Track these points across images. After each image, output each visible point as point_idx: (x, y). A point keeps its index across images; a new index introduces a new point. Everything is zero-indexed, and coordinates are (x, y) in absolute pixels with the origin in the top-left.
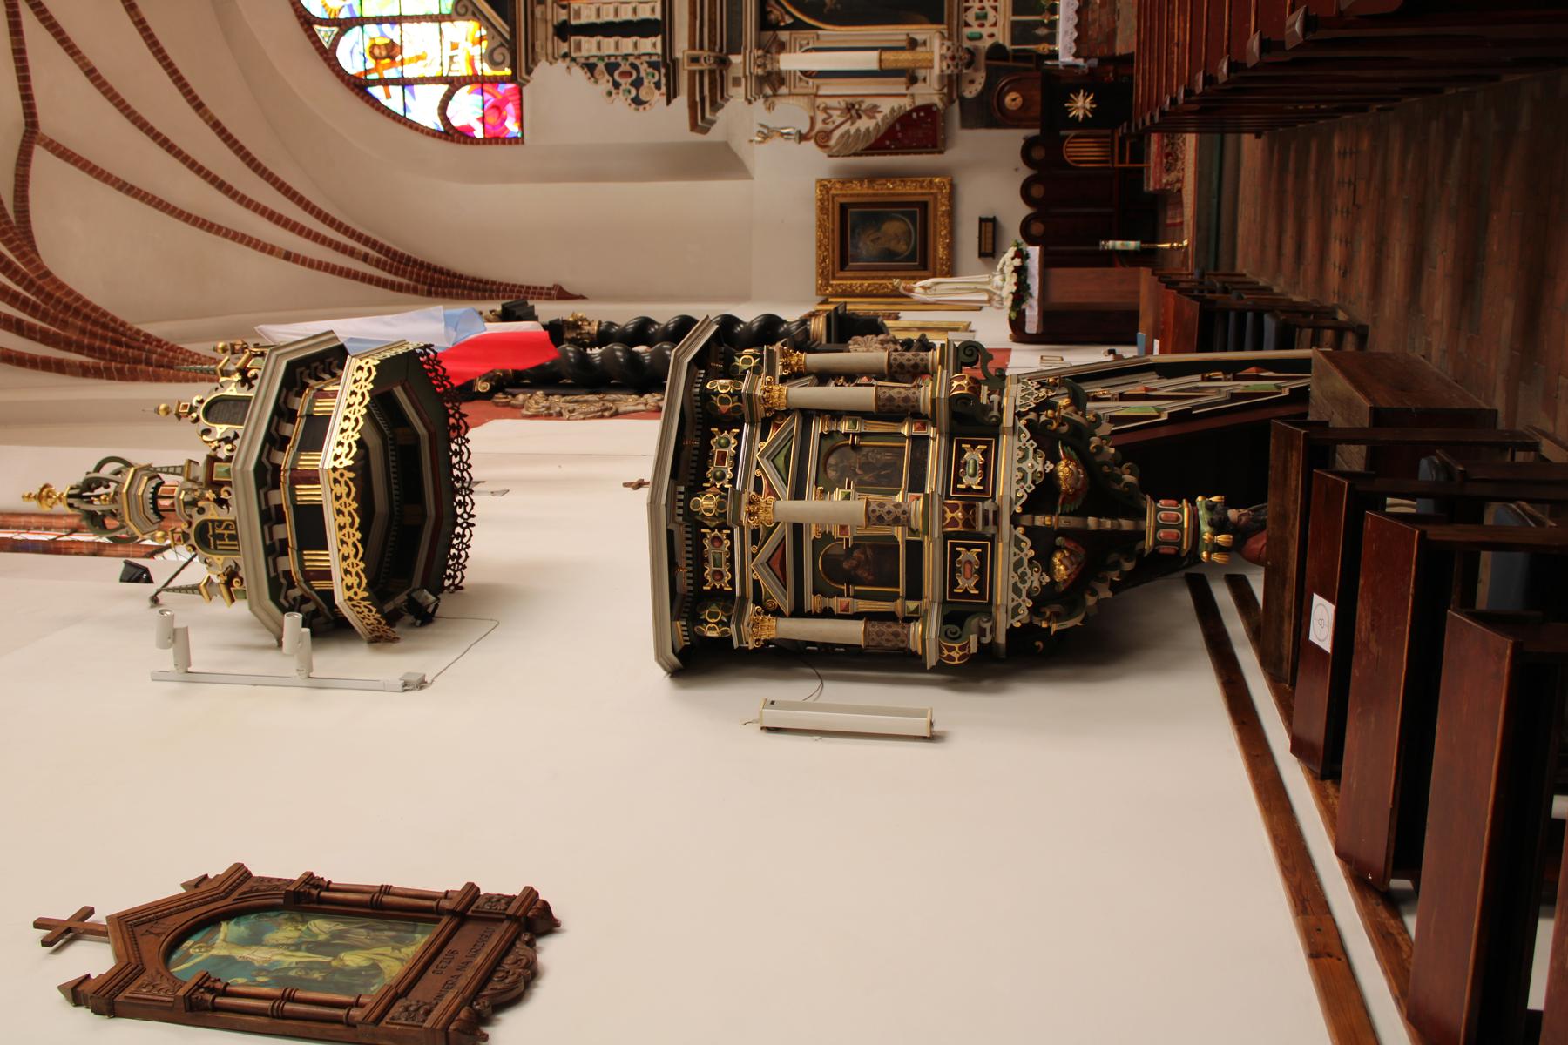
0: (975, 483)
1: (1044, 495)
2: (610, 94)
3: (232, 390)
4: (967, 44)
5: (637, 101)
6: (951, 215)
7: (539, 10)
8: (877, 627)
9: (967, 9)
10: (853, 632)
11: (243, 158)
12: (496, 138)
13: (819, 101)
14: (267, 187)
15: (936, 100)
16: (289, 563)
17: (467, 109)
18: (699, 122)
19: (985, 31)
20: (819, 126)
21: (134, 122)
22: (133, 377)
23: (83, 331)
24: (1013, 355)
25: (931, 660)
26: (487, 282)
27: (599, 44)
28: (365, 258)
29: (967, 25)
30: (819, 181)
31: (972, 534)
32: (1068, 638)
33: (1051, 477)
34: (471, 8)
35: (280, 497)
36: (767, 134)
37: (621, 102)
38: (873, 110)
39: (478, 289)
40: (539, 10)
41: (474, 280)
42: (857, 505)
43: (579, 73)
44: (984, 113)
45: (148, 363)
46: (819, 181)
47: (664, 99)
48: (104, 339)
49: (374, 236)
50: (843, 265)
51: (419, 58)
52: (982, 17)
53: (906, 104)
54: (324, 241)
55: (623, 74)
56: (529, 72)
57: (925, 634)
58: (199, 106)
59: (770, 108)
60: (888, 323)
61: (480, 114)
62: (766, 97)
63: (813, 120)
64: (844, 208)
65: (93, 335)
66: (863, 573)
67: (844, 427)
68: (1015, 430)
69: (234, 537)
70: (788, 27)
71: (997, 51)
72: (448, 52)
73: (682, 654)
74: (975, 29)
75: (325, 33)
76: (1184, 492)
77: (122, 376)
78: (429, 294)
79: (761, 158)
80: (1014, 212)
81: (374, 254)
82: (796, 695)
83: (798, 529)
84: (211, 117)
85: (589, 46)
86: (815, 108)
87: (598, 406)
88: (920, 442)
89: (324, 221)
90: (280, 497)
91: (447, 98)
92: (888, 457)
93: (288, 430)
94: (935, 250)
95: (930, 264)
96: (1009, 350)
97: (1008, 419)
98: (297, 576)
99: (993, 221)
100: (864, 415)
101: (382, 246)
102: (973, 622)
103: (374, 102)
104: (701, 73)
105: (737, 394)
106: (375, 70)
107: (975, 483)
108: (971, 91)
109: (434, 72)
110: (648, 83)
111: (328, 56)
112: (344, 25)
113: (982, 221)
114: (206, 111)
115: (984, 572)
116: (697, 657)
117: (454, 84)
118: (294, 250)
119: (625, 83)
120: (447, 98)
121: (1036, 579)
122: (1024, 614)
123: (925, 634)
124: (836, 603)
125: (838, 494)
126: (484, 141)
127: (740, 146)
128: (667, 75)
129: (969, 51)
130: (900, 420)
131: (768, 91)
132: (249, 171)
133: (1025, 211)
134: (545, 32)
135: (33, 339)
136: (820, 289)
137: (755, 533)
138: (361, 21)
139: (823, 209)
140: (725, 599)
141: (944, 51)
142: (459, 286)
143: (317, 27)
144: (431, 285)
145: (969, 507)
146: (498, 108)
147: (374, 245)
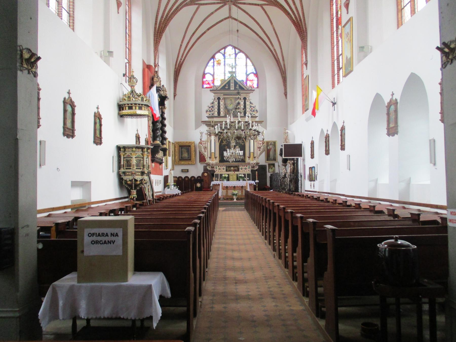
1: (136, 180)
3: (144, 99)
4: (215, 167)
5: (207, 111)
6: (189, 164)
7: (222, 95)
10: (122, 163)
17: (208, 78)
18: (204, 122)
19: (217, 170)
22: (154, 36)
28: (181, 59)
31: (132, 174)
32: (122, 183)
35: (133, 105)
36: (201, 133)
37: (207, 108)
38: (205, 151)
40: (222, 95)
43: (212, 101)
44: (206, 170)
50: (180, 146)
52: (220, 169)
53: (206, 157)
57: (122, 170)
58: (208, 29)
64: (190, 146)
71: (214, 171)
75: (222, 51)
76: (137, 194)
77: (155, 34)
80: (190, 175)
81: (182, 61)
85: (216, 103)
86: (206, 142)
88: (141, 169)
90: (133, 105)
91: (211, 74)
96: (162, 175)
99: (188, 171)
103: (210, 60)
108: (208, 168)
110: (210, 113)
111: (219, 51)
112: (224, 55)
116: (119, 148)
117: (213, 76)
120: (211, 74)
121: (128, 180)
123: (122, 170)
139: (190, 143)
140: (125, 151)
146: (209, 84)
147: (184, 61)
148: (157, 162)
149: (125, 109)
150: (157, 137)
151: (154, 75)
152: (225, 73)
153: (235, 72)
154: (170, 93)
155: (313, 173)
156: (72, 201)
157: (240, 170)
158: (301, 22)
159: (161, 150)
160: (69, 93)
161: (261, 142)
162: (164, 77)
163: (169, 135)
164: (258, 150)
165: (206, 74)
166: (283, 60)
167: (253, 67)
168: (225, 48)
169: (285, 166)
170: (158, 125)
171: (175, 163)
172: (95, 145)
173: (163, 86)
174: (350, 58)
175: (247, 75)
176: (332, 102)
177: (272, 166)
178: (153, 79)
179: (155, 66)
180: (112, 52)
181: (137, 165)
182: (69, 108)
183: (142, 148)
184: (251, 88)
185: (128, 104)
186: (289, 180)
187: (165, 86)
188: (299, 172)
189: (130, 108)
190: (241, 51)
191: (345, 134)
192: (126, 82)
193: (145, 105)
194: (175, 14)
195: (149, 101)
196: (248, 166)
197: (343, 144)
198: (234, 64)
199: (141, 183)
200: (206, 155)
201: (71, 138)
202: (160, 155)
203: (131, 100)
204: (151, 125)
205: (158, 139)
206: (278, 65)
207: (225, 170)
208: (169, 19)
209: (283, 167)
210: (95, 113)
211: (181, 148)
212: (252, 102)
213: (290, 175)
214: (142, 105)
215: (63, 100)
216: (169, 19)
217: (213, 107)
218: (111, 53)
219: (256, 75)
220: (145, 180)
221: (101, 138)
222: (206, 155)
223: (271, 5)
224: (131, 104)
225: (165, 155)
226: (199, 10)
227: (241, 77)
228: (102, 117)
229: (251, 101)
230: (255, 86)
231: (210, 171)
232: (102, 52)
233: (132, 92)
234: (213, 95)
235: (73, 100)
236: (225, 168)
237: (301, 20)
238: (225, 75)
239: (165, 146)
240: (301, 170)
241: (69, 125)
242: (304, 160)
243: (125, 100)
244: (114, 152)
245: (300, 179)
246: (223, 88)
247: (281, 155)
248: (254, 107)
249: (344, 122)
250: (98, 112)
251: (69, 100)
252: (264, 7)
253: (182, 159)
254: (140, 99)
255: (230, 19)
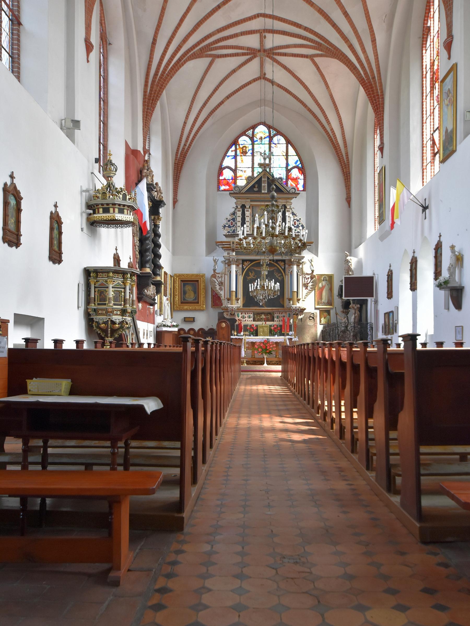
0: (115, 313)
1: (113, 323)
2: (227, 219)
3: (128, 197)
5: (225, 226)
6: (195, 310)
7: (249, 200)
8: (93, 299)
9: (245, 313)
10: (92, 296)
11: (215, 108)
12: (219, 183)
13: (224, 275)
14: (205, 116)
15: (224, 306)
16: (100, 206)
17: (227, 174)
20: (217, 275)
21: (203, 121)
22: (144, 105)
23: (155, 91)
24: (153, 325)
25: (88, 307)
26: (178, 180)
27: (240, 216)
28: (185, 145)
29: (242, 313)
30: (205, 274)
31: (107, 313)
33: (116, 324)
34: (250, 181)
35: (111, 206)
36: (215, 261)
37: (225, 222)
38: (221, 289)
39: (176, 178)
40: (249, 200)
41: (179, 176)
42: (111, 296)
44: (221, 318)
45: (148, 109)
46: (205, 274)
47: (225, 234)
48: (154, 96)
49: (191, 147)
51: (242, 161)
53: (223, 298)
54: (190, 133)
55: (232, 223)
56: (233, 197)
57: (92, 306)
58: (228, 97)
59: (222, 262)
60: (159, 295)
61: (226, 178)
62: (225, 261)
63: (219, 273)
65: (155, 93)
66: (101, 297)
67: (123, 294)
68: (123, 319)
69: (104, 199)
70: (243, 267)
72: (243, 169)
73: (88, 270)
74: (240, 316)
75: (250, 132)
77: (144, 102)
78: (175, 163)
79: (210, 259)
80: (196, 326)
81: (187, 147)
82: (82, 288)
83: (108, 287)
84: (225, 101)
85: (239, 214)
86: (222, 274)
87: (135, 232)
88: (121, 305)
89: (196, 133)
90: (111, 206)
92: (118, 300)
93: (122, 206)
94: (186, 306)
95: (182, 304)
97: (124, 317)
98: (98, 207)
99: (194, 321)
100: (125, 297)
101: (189, 150)
102: (94, 313)
104: (230, 245)
105: (127, 278)
106: (240, 148)
107: (115, 313)
109: (238, 165)
111: (244, 134)
113: (194, 318)
114: (226, 100)
115: (102, 314)
116: (88, 272)
118: (187, 125)
119: (229, 223)
121: (101, 322)
122: (96, 320)
123: (92, 306)
124: (96, 293)
125: (113, 293)
126: (219, 179)
127: (214, 254)
128: (231, 235)
129: (234, 314)
130: (124, 302)
131: (226, 262)
132: (209, 111)
133: (197, 329)
134: (243, 202)
135: (153, 78)
136: (175, 275)
137: (107, 281)
138: (253, 144)
139: (197, 275)
141: (234, 308)
142: (177, 172)
143: (252, 130)
144: (178, 164)
145: (111, 312)
146: (228, 184)
147: (189, 147)
148: (146, 302)
149: (98, 212)
150: (147, 262)
151: (144, 166)
152: (253, 168)
153: (269, 165)
154: (168, 197)
155: (391, 321)
156: (14, 345)
157: (275, 319)
158: (375, 81)
159: (153, 284)
160: (12, 177)
161: (309, 276)
162: (158, 170)
163: (165, 262)
164: (304, 288)
165: (225, 168)
166: (346, 146)
167: (296, 158)
168: (254, 127)
169: (347, 313)
170: (148, 244)
171: (173, 309)
172: (51, 263)
173: (157, 184)
174: (452, 131)
175: (288, 171)
176: (422, 206)
177: (326, 314)
178: (141, 172)
179: (145, 153)
180: (78, 122)
181: (116, 299)
182: (13, 202)
183: (123, 273)
184: (293, 191)
185: (102, 205)
186: (352, 334)
187: (160, 185)
188: (369, 321)
189: (106, 211)
190: (279, 133)
191: (441, 254)
192: (100, 172)
193: (129, 206)
194: (177, 71)
195: (135, 200)
196: (288, 313)
197: (439, 270)
198: (267, 153)
199: (122, 327)
200: (223, 295)
201: (14, 248)
202: (151, 290)
203: (107, 197)
204: (138, 243)
205: (148, 266)
206: (337, 154)
207: (252, 319)
208: (166, 78)
209: (344, 315)
210: (51, 213)
211: (184, 285)
212: (295, 212)
213: (354, 327)
214: (124, 206)
215: (3, 186)
216: (166, 78)
217: (233, 219)
218: (76, 124)
219: (302, 170)
220: (127, 324)
221: (60, 253)
222: (223, 295)
223: (327, 56)
224: (108, 204)
225: (158, 291)
226: (213, 66)
227: (278, 172)
228: (63, 220)
229: (294, 210)
230: (301, 187)
231: (229, 320)
232: (63, 121)
233: (110, 186)
234: (235, 201)
235: (18, 188)
236: (252, 315)
237: (374, 78)
238: (253, 171)
239: (158, 278)
240: (371, 318)
241: (12, 226)
242: (376, 302)
243: (98, 197)
244: (79, 278)
245: (369, 333)
246: (251, 190)
247: (340, 295)
248: (298, 221)
249: (440, 236)
250: (56, 211)
251: (12, 188)
252: (316, 59)
253: (184, 302)
254: (121, 196)
255: (263, 81)
